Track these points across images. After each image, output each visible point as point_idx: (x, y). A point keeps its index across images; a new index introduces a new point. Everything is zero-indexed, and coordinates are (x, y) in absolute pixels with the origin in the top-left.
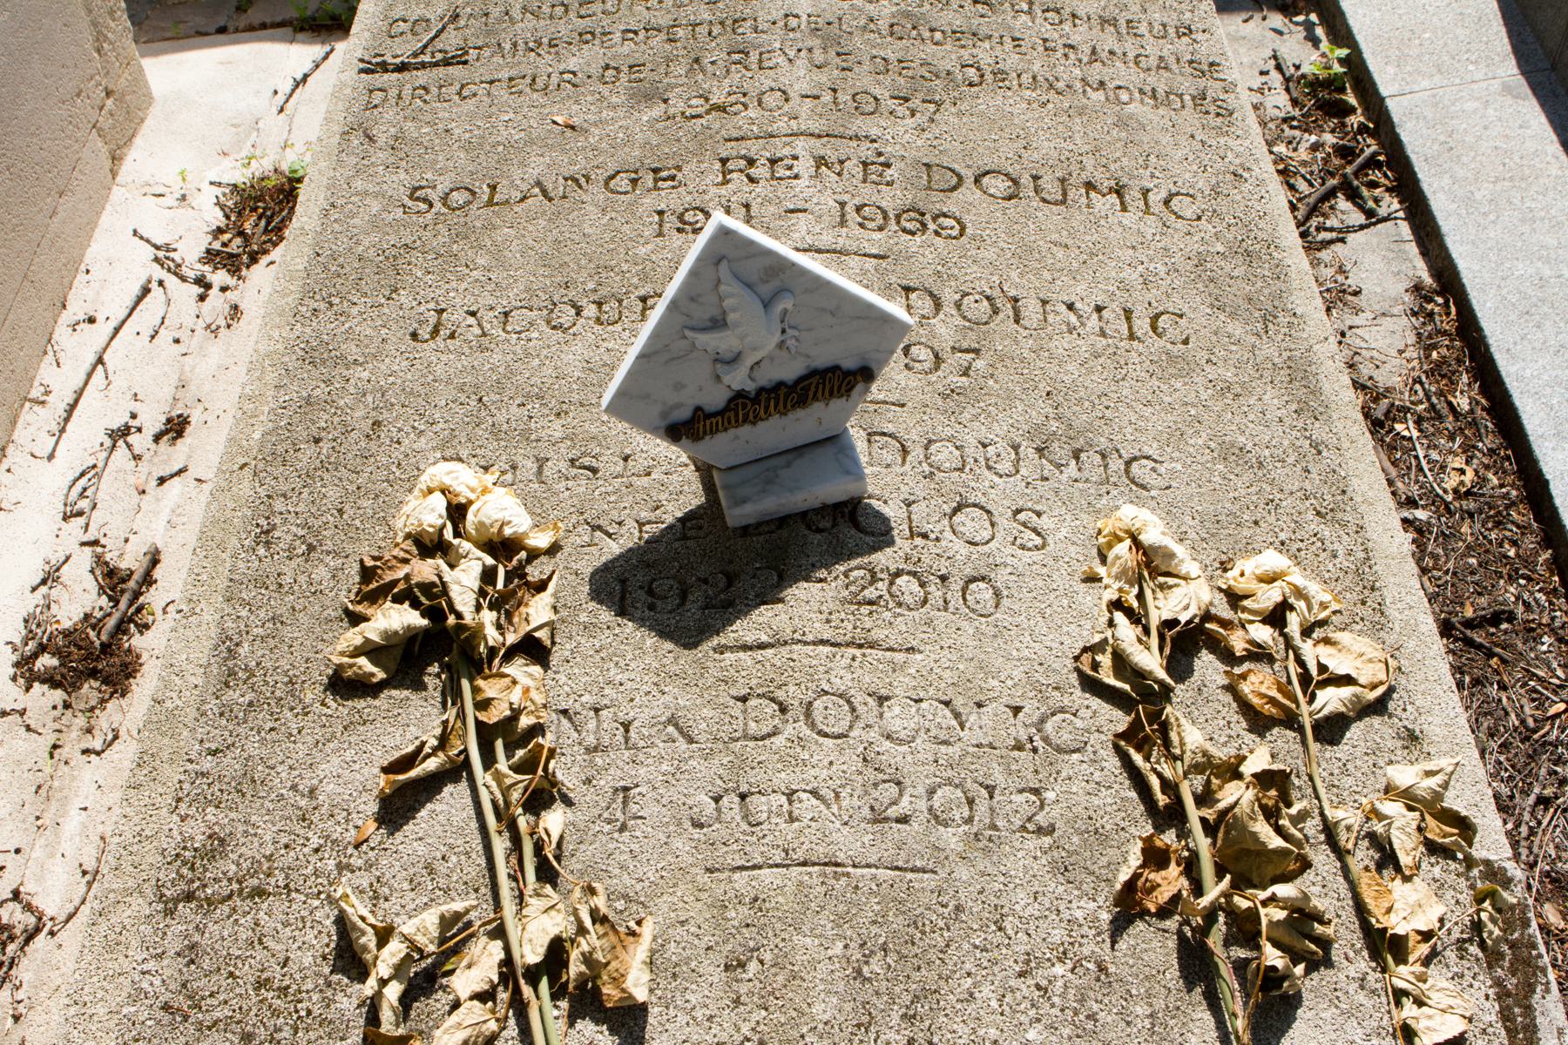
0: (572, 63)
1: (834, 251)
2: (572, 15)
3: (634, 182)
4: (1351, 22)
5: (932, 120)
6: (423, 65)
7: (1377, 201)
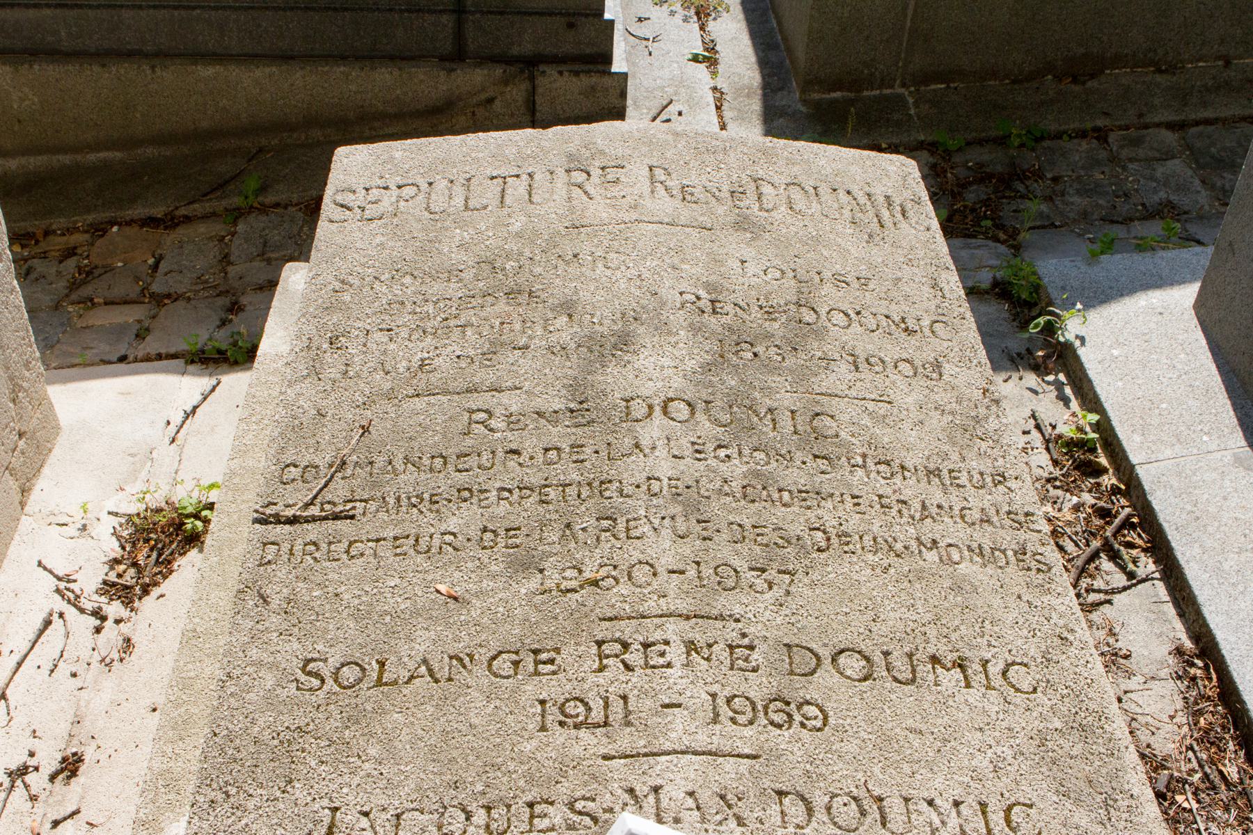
0: (452, 524)
1: (710, 753)
2: (450, 468)
3: (516, 664)
4: (1098, 390)
5: (788, 593)
6: (314, 519)
7: (1135, 562)
